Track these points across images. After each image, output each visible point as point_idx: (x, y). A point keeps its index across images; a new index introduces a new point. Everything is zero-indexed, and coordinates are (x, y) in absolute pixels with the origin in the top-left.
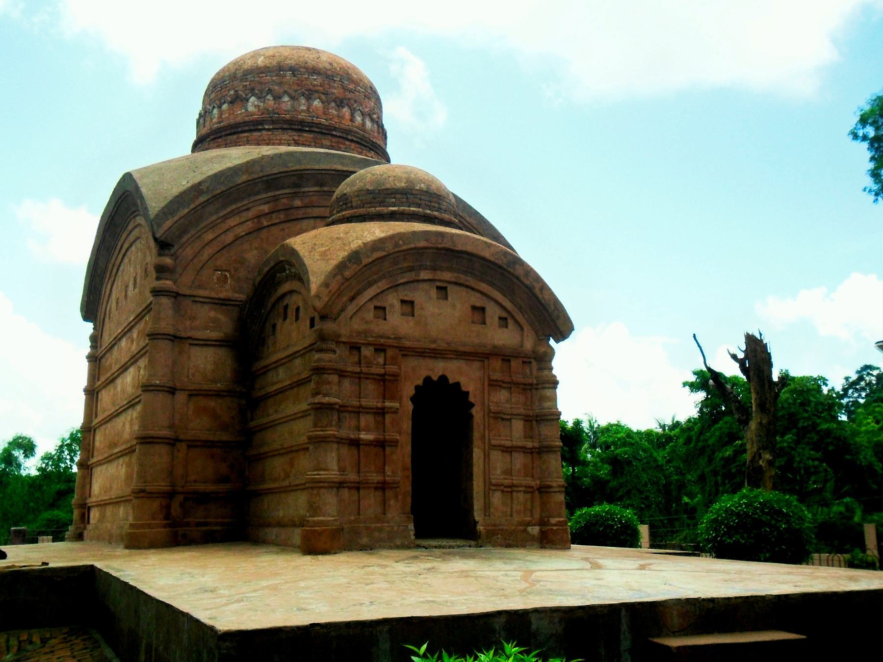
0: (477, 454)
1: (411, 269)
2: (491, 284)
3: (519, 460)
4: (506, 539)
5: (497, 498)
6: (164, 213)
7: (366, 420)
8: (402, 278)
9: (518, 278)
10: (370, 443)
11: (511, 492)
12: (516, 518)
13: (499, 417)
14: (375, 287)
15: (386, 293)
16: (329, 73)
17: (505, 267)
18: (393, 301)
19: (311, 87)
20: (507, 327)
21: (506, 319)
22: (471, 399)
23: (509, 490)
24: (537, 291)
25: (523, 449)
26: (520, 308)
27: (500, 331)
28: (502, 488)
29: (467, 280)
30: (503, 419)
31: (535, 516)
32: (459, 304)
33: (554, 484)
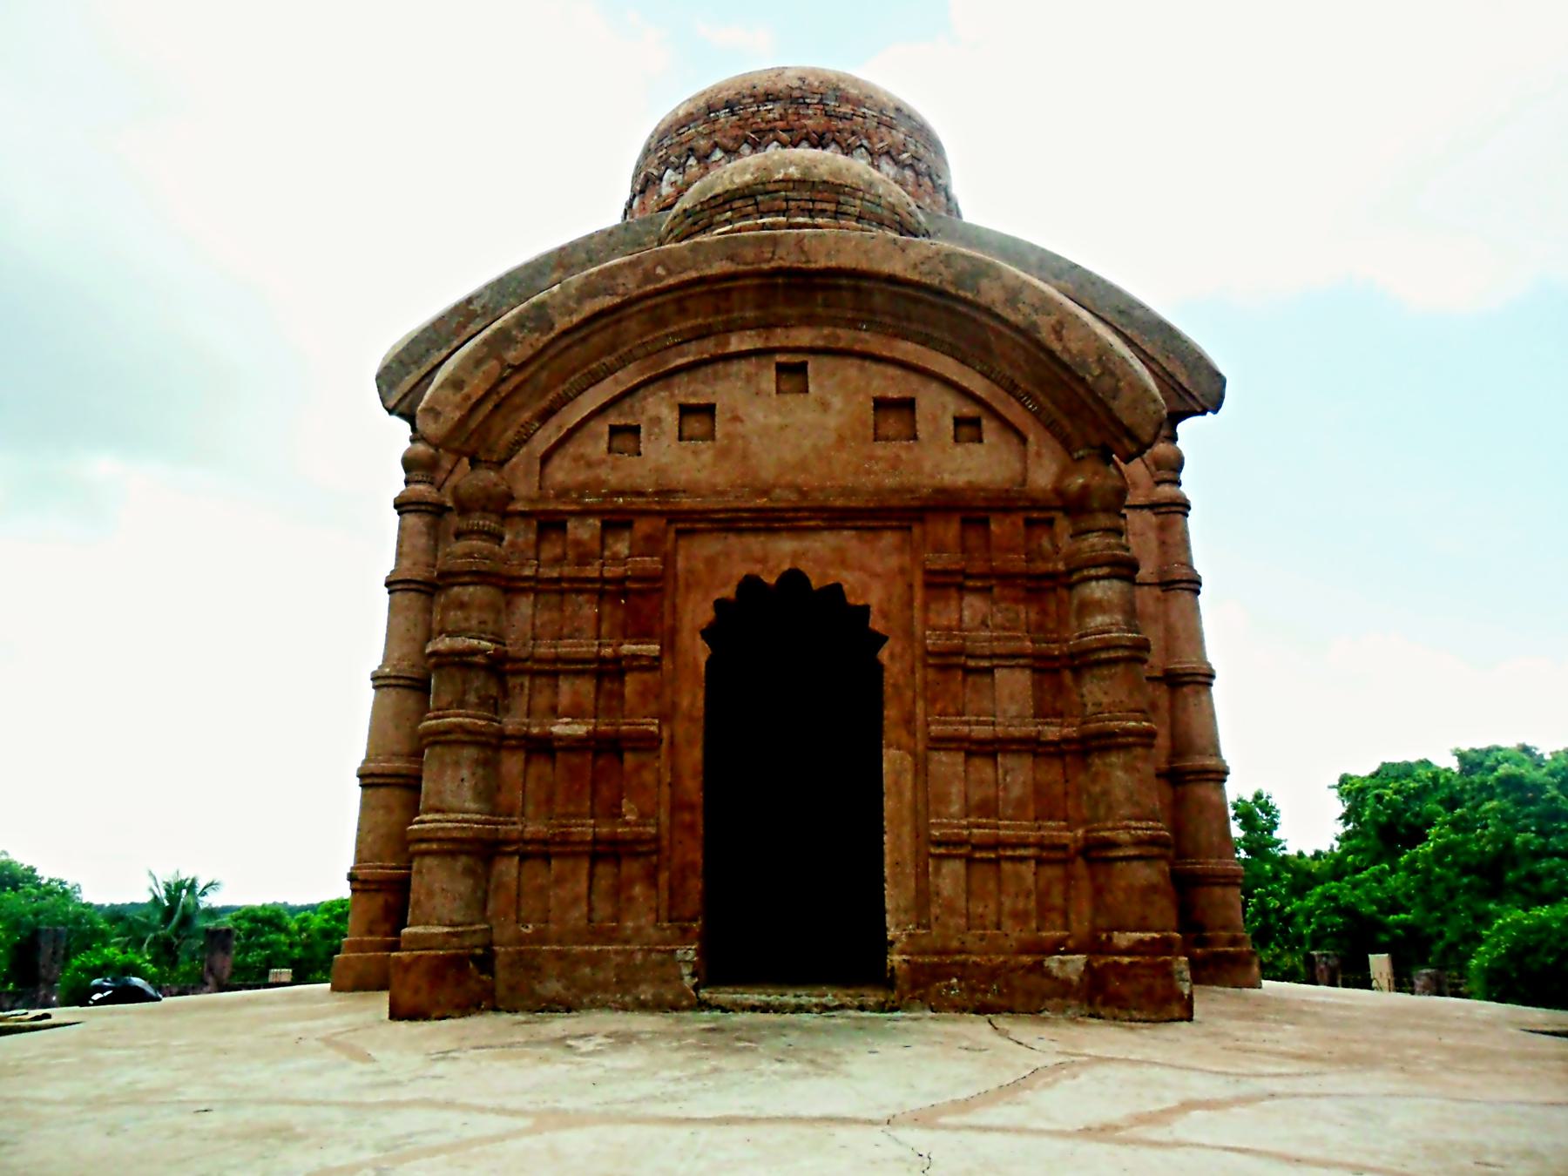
0: (893, 761)
1: (700, 334)
2: (926, 341)
3: (1017, 776)
4: (973, 990)
5: (949, 878)
6: (401, 362)
7: (568, 690)
8: (682, 355)
9: (988, 311)
10: (575, 745)
11: (996, 862)
12: (1015, 933)
13: (954, 665)
14: (608, 381)
15: (641, 392)
16: (796, 93)
17: (952, 290)
18: (660, 408)
19: (763, 126)
20: (980, 441)
21: (975, 422)
22: (876, 624)
23: (983, 857)
24: (1046, 336)
25: (1032, 747)
26: (1012, 389)
27: (959, 450)
28: (962, 851)
29: (861, 341)
30: (968, 671)
31: (1074, 925)
32: (836, 401)
33: (1123, 836)
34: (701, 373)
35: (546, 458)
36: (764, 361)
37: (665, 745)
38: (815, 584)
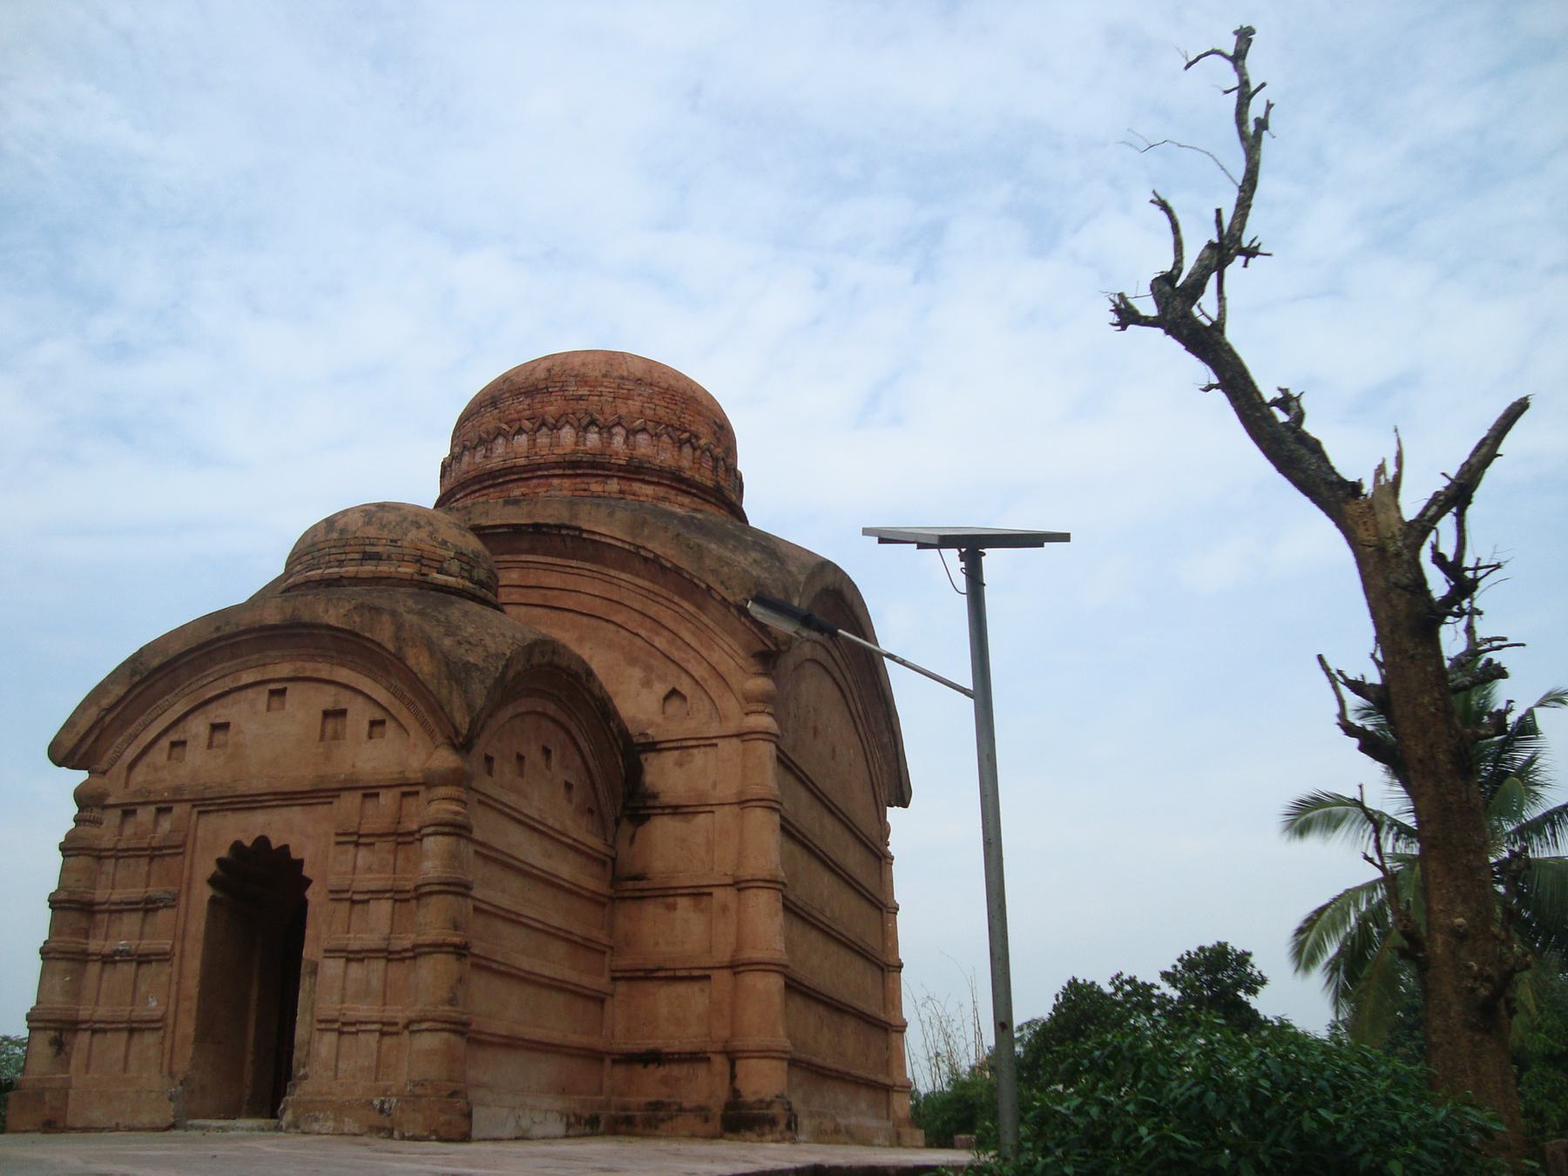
9: (379, 645)
13: (354, 900)
18: (198, 727)
21: (382, 723)
22: (307, 871)
28: (336, 1026)
30: (354, 902)
32: (305, 706)
34: (224, 701)
35: (132, 766)
36: (261, 688)
37: (176, 959)
38: (248, 843)
